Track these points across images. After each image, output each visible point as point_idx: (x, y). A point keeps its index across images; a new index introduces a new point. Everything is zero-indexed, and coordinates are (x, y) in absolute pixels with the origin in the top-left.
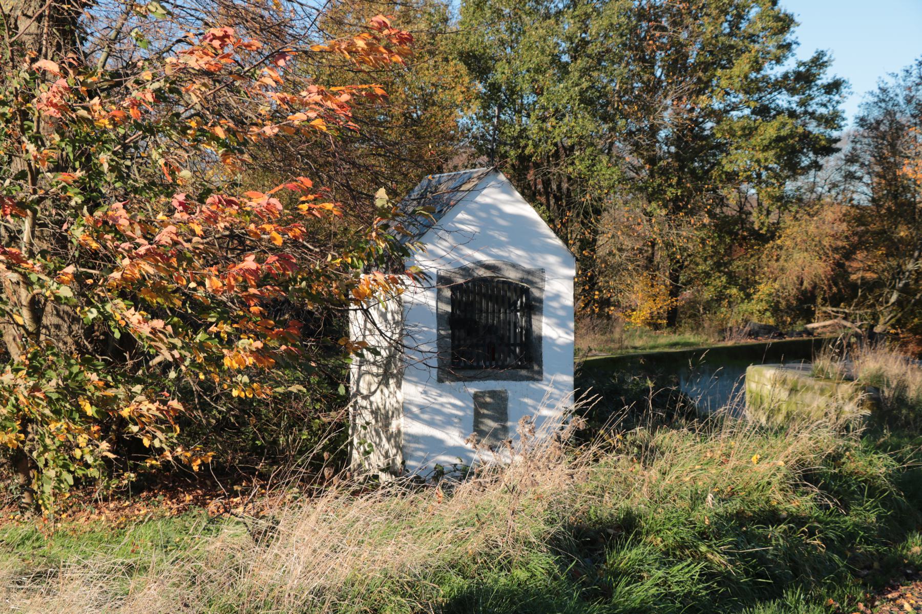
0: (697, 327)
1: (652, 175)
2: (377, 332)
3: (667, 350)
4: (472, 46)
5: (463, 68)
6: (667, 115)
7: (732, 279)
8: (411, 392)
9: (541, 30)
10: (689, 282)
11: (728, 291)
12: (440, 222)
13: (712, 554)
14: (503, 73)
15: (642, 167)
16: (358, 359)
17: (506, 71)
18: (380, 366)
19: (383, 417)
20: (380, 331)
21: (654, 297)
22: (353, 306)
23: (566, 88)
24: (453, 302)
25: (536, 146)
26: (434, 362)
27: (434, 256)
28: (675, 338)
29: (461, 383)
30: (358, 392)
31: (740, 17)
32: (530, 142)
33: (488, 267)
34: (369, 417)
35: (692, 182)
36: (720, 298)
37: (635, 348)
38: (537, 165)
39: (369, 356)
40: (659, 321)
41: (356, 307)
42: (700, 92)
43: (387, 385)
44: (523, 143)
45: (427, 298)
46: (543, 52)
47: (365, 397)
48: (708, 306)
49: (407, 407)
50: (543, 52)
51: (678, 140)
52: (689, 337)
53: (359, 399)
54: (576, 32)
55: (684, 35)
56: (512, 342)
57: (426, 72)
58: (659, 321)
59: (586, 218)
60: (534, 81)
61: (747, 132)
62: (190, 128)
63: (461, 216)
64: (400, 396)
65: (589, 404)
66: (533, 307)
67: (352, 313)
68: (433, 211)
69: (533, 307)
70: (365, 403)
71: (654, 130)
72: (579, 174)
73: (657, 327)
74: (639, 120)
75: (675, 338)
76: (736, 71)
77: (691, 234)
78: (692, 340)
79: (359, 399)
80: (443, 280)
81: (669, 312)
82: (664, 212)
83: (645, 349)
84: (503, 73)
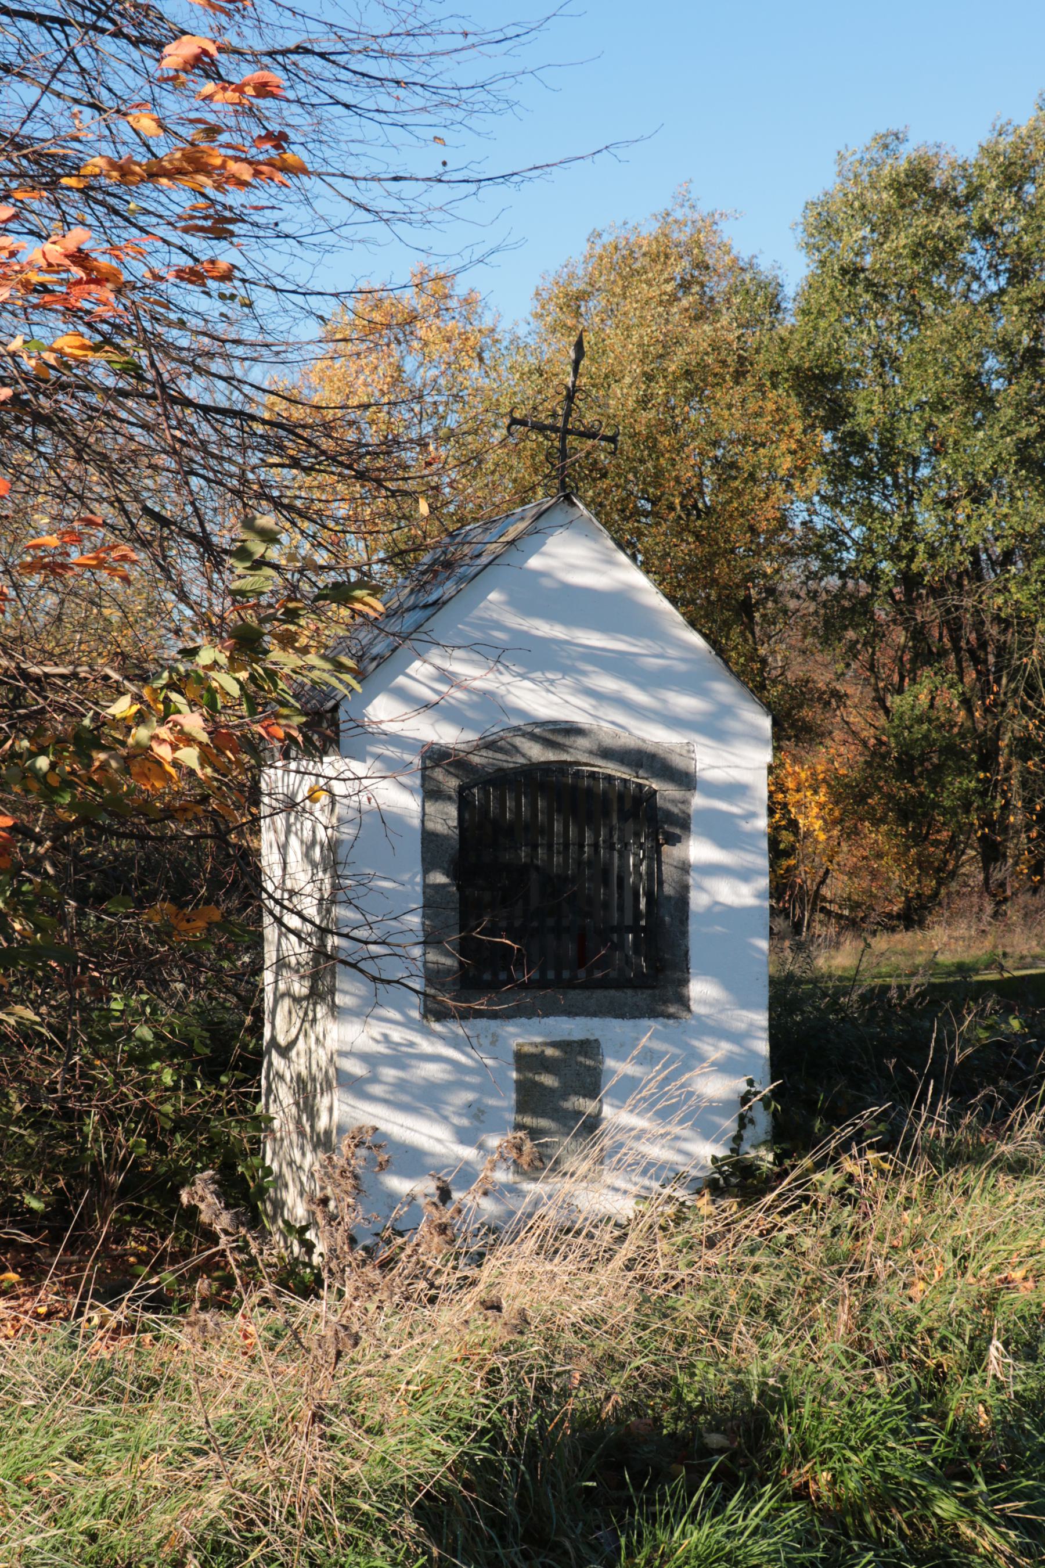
9: (944, 327)
13: (972, 1525)
25: (932, 555)
29: (498, 1022)
32: (921, 547)
44: (905, 548)
46: (947, 369)
54: (1020, 333)
57: (726, 413)
59: (1031, 698)
60: (931, 426)
62: (382, 561)
69: (664, 826)
72: (1018, 610)
80: (436, 757)
84: (870, 411)
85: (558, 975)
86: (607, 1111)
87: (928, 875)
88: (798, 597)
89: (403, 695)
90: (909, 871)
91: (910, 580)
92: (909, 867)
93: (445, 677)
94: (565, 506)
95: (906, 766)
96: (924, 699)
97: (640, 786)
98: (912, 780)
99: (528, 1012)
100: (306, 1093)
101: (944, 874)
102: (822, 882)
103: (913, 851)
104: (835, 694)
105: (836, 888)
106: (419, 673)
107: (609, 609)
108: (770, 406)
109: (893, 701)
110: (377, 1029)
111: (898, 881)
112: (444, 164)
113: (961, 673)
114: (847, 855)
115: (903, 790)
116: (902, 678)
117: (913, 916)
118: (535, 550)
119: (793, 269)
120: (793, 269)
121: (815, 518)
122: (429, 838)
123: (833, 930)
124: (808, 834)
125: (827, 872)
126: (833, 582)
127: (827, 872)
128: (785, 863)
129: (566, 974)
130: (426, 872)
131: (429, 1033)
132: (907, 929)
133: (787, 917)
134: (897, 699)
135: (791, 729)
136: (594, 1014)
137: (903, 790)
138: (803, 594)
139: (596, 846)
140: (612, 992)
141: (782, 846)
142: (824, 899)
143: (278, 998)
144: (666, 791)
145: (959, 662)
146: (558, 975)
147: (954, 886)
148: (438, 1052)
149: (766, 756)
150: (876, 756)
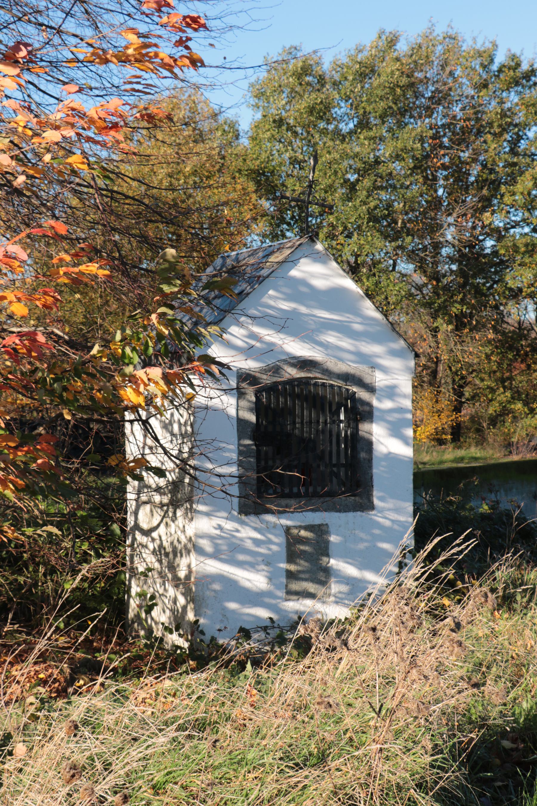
0: (481, 441)
1: (436, 293)
2: (160, 450)
3: (455, 465)
4: (262, 163)
5: (252, 187)
6: (450, 234)
7: (517, 395)
8: (203, 524)
10: (474, 397)
11: (513, 406)
12: (241, 306)
15: (425, 285)
16: (136, 483)
18: (164, 494)
19: (169, 555)
20: (164, 449)
21: (439, 412)
22: (128, 416)
23: (355, 206)
24: (258, 408)
26: (235, 490)
27: (233, 346)
28: (461, 453)
30: (137, 527)
31: (519, 138)
33: (304, 364)
34: (151, 560)
35: (476, 297)
36: (505, 412)
37: (424, 463)
39: (151, 479)
40: (444, 437)
41: (132, 417)
42: (483, 209)
43: (174, 518)
45: (229, 404)
47: (147, 533)
48: (493, 421)
49: (198, 547)
51: (460, 258)
52: (474, 451)
53: (138, 536)
55: (465, 155)
56: (334, 461)
58: (444, 437)
61: (530, 248)
64: (190, 531)
65: (461, 552)
66: (361, 413)
67: (128, 425)
68: (232, 290)
70: (144, 540)
71: (437, 246)
73: (441, 442)
74: (421, 237)
75: (461, 453)
76: (519, 187)
77: (475, 350)
78: (478, 455)
79: (138, 536)
80: (246, 377)
81: (453, 427)
82: (450, 327)
83: (433, 464)
85: (307, 490)
93: (253, 336)
97: (348, 390)
106: (236, 333)
107: (333, 298)
108: (239, 187)
110: (216, 521)
112: (225, 58)
119: (246, 118)
120: (246, 118)
122: (241, 422)
129: (295, 490)
130: (239, 439)
131: (243, 523)
139: (325, 422)
143: (139, 504)
144: (362, 394)
146: (291, 490)
148: (247, 532)
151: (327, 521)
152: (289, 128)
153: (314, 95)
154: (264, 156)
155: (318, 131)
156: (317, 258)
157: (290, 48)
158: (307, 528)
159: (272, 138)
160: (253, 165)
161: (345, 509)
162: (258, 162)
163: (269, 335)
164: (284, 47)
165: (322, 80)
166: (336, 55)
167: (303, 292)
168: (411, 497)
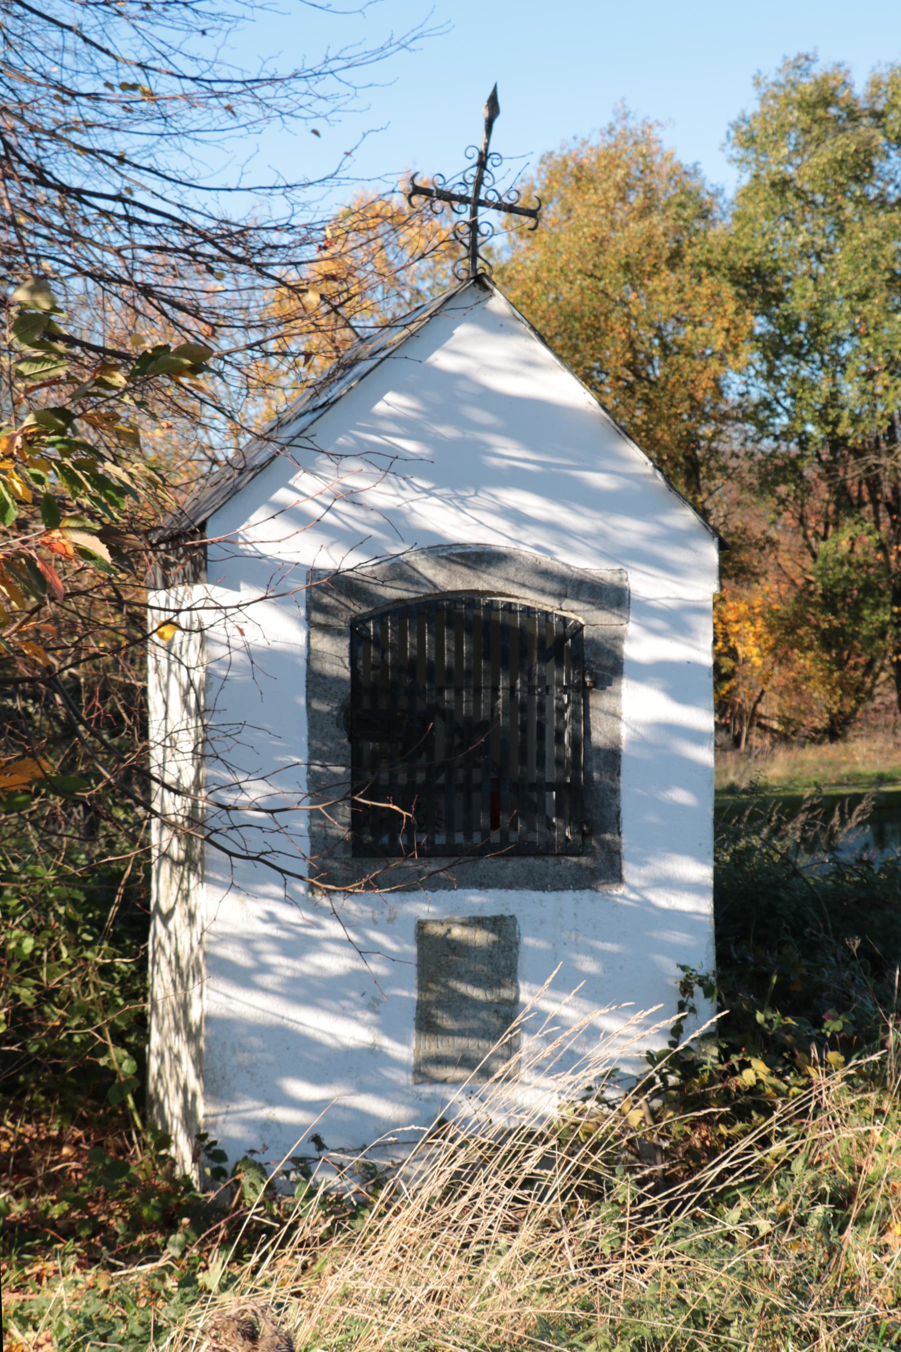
5: (728, 290)
14: (803, 297)
17: (808, 294)
25: (856, 420)
38: (858, 453)
50: (875, 264)
63: (393, 402)
69: (597, 666)
86: (524, 997)
87: (849, 695)
88: (737, 457)
89: (283, 511)
90: (832, 692)
91: (836, 443)
92: (833, 688)
94: (476, 290)
95: (829, 602)
96: (845, 545)
97: (564, 620)
98: (835, 613)
99: (433, 884)
100: (182, 976)
101: (861, 693)
102: (759, 700)
103: (836, 675)
104: (770, 541)
105: (769, 708)
106: (308, 487)
107: (528, 418)
109: (822, 547)
110: (258, 907)
111: (822, 700)
113: (877, 523)
114: (780, 675)
115: (827, 621)
116: (826, 528)
117: (836, 730)
118: (437, 345)
119: (724, 176)
120: (724, 176)
121: (752, 389)
123: (767, 741)
124: (745, 661)
125: (763, 692)
126: (768, 444)
127: (763, 692)
128: (727, 686)
132: (832, 741)
133: (728, 731)
134: (822, 545)
135: (734, 568)
136: (510, 886)
137: (827, 621)
138: (742, 454)
140: (531, 860)
141: (723, 671)
142: (761, 716)
145: (876, 513)
147: (870, 705)
149: (715, 588)
150: (804, 594)
151: (513, 910)
152: (800, 194)
153: (842, 140)
154: (759, 244)
155: (851, 199)
156: (497, 326)
157: (799, 57)
158: (477, 922)
159: (770, 213)
160: (742, 261)
161: (558, 884)
162: (749, 255)
163: (382, 495)
164: (785, 57)
165: (853, 116)
166: (873, 69)
167: (454, 396)
168: (712, 855)
